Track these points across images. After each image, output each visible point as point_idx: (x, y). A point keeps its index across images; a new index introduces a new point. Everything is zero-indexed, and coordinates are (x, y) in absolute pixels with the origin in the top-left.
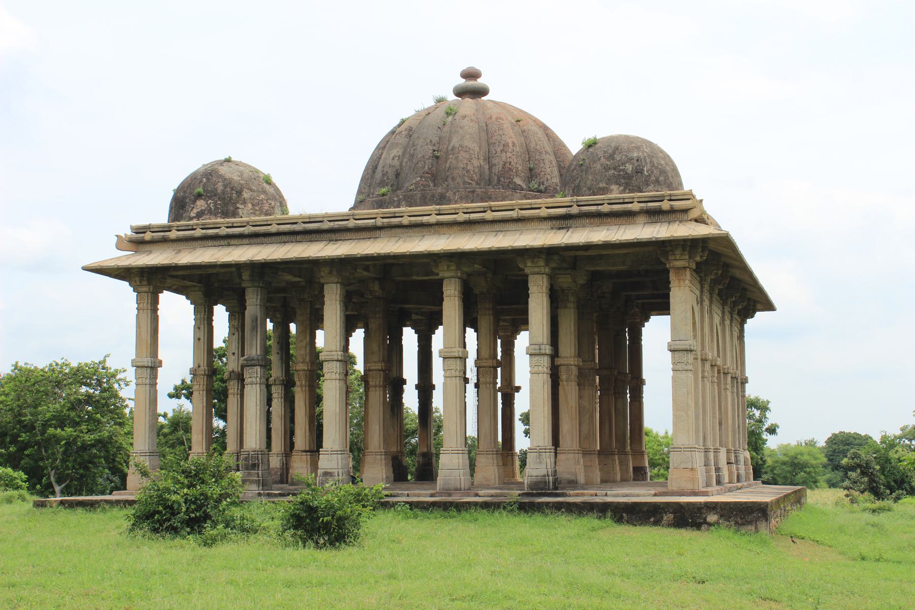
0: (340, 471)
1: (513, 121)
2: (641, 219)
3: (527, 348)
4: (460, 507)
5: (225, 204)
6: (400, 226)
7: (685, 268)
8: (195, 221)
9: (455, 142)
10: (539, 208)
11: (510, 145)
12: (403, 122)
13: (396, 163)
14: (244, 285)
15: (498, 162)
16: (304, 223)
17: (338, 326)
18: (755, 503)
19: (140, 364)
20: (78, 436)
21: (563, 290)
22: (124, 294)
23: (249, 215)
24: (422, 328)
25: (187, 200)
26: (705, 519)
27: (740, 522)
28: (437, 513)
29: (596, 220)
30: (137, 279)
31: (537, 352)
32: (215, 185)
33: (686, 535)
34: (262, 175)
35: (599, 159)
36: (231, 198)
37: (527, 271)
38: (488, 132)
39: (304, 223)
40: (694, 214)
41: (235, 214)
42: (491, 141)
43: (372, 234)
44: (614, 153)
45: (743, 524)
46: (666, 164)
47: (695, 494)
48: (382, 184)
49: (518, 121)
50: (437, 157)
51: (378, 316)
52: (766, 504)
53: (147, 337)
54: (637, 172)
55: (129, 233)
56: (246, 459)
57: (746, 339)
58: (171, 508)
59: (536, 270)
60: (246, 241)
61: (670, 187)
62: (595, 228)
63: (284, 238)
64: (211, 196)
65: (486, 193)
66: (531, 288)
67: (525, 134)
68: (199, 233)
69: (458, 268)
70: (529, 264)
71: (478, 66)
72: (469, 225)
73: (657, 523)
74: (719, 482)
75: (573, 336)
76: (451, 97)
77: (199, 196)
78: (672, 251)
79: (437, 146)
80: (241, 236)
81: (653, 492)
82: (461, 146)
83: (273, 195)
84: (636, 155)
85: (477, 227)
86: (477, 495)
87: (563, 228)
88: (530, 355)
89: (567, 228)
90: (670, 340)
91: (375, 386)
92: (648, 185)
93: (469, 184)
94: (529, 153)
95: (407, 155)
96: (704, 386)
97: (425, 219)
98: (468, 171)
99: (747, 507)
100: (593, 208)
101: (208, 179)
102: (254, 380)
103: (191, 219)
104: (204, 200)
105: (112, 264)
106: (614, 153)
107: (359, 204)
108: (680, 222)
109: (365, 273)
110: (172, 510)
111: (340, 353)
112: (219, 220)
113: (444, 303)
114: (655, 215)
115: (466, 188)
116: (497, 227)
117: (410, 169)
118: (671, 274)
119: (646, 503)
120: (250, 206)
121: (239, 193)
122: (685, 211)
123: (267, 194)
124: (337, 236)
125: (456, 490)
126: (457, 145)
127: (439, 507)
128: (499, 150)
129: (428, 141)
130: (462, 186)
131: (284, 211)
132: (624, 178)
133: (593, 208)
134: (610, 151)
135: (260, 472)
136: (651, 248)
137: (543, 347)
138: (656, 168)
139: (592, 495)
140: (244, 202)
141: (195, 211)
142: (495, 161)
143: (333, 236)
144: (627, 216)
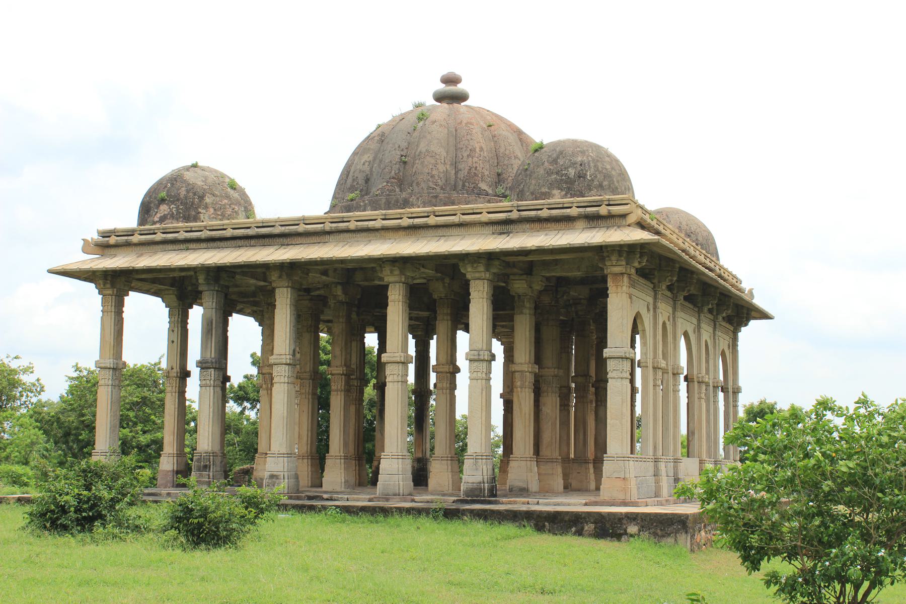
0: (286, 474)
1: (485, 126)
2: (580, 224)
3: (467, 354)
4: (386, 512)
5: (187, 209)
6: (348, 231)
7: (622, 274)
8: (158, 226)
9: (422, 147)
10: (481, 213)
11: (478, 150)
12: (379, 126)
13: (366, 168)
14: (200, 289)
15: (464, 167)
16: (257, 227)
17: (288, 330)
18: (676, 514)
19: (103, 365)
20: (134, 437)
21: (519, 296)
22: (90, 296)
23: (211, 219)
24: (419, 333)
25: (152, 205)
26: (625, 530)
27: (659, 532)
28: (365, 518)
29: (537, 225)
30: (101, 282)
31: (476, 358)
32: (178, 189)
33: (605, 546)
34: (227, 180)
35: (543, 164)
36: (193, 203)
37: (468, 276)
38: (457, 138)
39: (257, 227)
40: (632, 219)
41: (196, 219)
42: (459, 146)
43: (323, 238)
44: (558, 157)
45: (664, 536)
46: (612, 168)
47: (625, 504)
48: (352, 189)
49: (490, 126)
50: (405, 163)
51: (341, 320)
52: (687, 516)
53: (110, 339)
54: (580, 177)
55: (96, 237)
56: (199, 460)
57: (740, 348)
58: (63, 507)
59: (477, 275)
60: (204, 245)
61: (615, 191)
62: (534, 234)
63: (239, 242)
64: (176, 201)
65: (449, 198)
66: (472, 294)
67: (495, 139)
68: (159, 237)
69: (402, 273)
70: (469, 269)
71: (458, 72)
72: (413, 230)
73: (580, 533)
74: (657, 495)
75: (528, 342)
76: (430, 102)
77: (163, 201)
78: (608, 256)
79: (405, 151)
80: (198, 240)
81: (584, 502)
82: (427, 151)
83: (237, 199)
84: (579, 159)
85: (422, 232)
86: (413, 501)
87: (504, 233)
88: (470, 361)
89: (508, 233)
90: (468, 350)
91: (337, 390)
92: (590, 190)
93: (433, 189)
94: (498, 157)
95: (377, 161)
96: (655, 394)
97: (371, 224)
98: (432, 176)
99: (668, 519)
100: (533, 213)
101: (172, 184)
102: (208, 382)
103: (154, 223)
104: (167, 204)
105: (74, 267)
106: (558, 157)
107: (333, 207)
108: (619, 227)
109: (324, 278)
110: (63, 510)
111: (288, 357)
112: (181, 224)
113: (276, 311)
114: (594, 220)
115: (429, 193)
116: (440, 232)
117: (381, 175)
118: (609, 280)
119: (568, 512)
120: (212, 210)
121: (202, 198)
122: (624, 216)
123: (234, 197)
124: (289, 240)
125: (395, 495)
126: (424, 150)
127: (367, 511)
128: (465, 155)
129: (397, 146)
130: (425, 191)
131: (254, 217)
132: (566, 183)
133: (533, 213)
134: (555, 156)
135: (211, 474)
136: (590, 254)
137: (481, 353)
138: (600, 172)
139: (523, 503)
140: (206, 207)
141: (158, 215)
142: (461, 166)
143: (285, 241)
144: (565, 221)
